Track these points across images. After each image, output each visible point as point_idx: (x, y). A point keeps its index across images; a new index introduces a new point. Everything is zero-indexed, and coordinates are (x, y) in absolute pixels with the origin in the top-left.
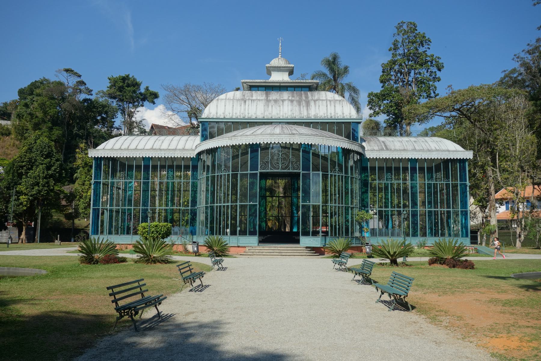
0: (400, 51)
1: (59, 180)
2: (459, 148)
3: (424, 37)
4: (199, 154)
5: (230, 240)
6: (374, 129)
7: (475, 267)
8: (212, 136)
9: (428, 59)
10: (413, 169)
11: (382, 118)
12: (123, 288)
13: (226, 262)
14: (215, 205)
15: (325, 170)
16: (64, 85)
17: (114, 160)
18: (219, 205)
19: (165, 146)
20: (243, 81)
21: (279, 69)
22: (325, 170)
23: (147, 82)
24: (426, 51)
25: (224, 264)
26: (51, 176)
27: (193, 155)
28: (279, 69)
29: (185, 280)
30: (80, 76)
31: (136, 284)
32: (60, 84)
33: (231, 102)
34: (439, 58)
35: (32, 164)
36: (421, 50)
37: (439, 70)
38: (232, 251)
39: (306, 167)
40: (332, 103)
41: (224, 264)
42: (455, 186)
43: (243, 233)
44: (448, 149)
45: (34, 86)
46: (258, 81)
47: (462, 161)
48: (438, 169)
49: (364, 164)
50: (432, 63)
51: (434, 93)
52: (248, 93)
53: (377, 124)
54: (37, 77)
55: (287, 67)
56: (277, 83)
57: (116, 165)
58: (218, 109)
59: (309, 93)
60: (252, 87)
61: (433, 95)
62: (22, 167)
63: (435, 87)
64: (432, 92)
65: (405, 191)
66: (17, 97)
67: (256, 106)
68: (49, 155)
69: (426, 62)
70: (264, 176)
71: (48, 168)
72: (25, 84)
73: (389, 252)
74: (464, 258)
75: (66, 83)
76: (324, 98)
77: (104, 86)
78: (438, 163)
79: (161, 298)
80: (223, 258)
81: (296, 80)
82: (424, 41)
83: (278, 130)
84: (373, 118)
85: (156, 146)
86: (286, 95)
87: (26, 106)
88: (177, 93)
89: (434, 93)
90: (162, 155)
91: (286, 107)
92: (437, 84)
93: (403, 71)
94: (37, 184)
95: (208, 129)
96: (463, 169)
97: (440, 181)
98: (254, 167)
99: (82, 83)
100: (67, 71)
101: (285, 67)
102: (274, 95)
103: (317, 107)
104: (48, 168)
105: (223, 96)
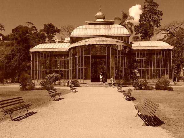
0: (147, 9)
1: (23, 60)
2: (168, 45)
3: (156, 3)
4: (70, 49)
5: (80, 81)
6: (136, 39)
7: (173, 89)
8: (75, 42)
9: (157, 12)
10: (150, 54)
11: (139, 35)
12: (7, 102)
13: (78, 89)
14: (80, 68)
15: (116, 54)
16: (27, 27)
17: (39, 53)
18: (76, 68)
19: (57, 47)
20: (86, 21)
21: (100, 17)
22: (116, 54)
23: (57, 26)
24: (156, 9)
25: (76, 90)
26: (21, 59)
27: (67, 50)
28: (100, 17)
29: (52, 96)
30: (33, 24)
31: (18, 99)
32: (26, 27)
33: (82, 29)
34: (162, 11)
35: (14, 55)
36: (155, 8)
37: (162, 16)
38: (81, 85)
39: (109, 53)
40: (119, 28)
41: (76, 90)
42: (166, 60)
43: (85, 78)
44: (165, 45)
45: (17, 28)
46: (92, 21)
47: (170, 50)
48: (160, 53)
49: (132, 53)
50: (159, 13)
51: (159, 25)
52: (87, 26)
53: (138, 38)
54: (18, 25)
55: (103, 16)
56: (99, 22)
57: (40, 54)
58: (76, 32)
59: (111, 25)
60: (90, 24)
61: (159, 25)
62: (11, 56)
63: (160, 23)
64: (158, 24)
65: (148, 62)
66: (12, 33)
67: (90, 31)
68: (20, 52)
69: (157, 13)
70: (93, 57)
71: (20, 56)
72: (14, 28)
73: (139, 84)
74: (169, 86)
75: (28, 27)
76: (116, 27)
77: (42, 27)
78: (160, 51)
79: (29, 105)
80: (76, 88)
81: (107, 20)
82: (156, 5)
83: (98, 39)
84: (136, 35)
85: (54, 47)
86: (102, 26)
87: (14, 35)
88: (64, 28)
89: (159, 25)
90: (56, 50)
91: (102, 30)
92: (160, 21)
93: (148, 17)
94: (16, 62)
95: (74, 40)
96: (170, 54)
97: (161, 57)
98: (89, 53)
99: (34, 27)
100: (29, 22)
101: (102, 16)
102: (98, 26)
103: (114, 30)
104: (20, 56)
105: (78, 28)
